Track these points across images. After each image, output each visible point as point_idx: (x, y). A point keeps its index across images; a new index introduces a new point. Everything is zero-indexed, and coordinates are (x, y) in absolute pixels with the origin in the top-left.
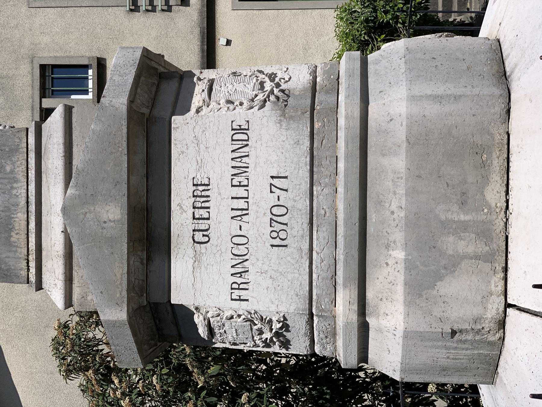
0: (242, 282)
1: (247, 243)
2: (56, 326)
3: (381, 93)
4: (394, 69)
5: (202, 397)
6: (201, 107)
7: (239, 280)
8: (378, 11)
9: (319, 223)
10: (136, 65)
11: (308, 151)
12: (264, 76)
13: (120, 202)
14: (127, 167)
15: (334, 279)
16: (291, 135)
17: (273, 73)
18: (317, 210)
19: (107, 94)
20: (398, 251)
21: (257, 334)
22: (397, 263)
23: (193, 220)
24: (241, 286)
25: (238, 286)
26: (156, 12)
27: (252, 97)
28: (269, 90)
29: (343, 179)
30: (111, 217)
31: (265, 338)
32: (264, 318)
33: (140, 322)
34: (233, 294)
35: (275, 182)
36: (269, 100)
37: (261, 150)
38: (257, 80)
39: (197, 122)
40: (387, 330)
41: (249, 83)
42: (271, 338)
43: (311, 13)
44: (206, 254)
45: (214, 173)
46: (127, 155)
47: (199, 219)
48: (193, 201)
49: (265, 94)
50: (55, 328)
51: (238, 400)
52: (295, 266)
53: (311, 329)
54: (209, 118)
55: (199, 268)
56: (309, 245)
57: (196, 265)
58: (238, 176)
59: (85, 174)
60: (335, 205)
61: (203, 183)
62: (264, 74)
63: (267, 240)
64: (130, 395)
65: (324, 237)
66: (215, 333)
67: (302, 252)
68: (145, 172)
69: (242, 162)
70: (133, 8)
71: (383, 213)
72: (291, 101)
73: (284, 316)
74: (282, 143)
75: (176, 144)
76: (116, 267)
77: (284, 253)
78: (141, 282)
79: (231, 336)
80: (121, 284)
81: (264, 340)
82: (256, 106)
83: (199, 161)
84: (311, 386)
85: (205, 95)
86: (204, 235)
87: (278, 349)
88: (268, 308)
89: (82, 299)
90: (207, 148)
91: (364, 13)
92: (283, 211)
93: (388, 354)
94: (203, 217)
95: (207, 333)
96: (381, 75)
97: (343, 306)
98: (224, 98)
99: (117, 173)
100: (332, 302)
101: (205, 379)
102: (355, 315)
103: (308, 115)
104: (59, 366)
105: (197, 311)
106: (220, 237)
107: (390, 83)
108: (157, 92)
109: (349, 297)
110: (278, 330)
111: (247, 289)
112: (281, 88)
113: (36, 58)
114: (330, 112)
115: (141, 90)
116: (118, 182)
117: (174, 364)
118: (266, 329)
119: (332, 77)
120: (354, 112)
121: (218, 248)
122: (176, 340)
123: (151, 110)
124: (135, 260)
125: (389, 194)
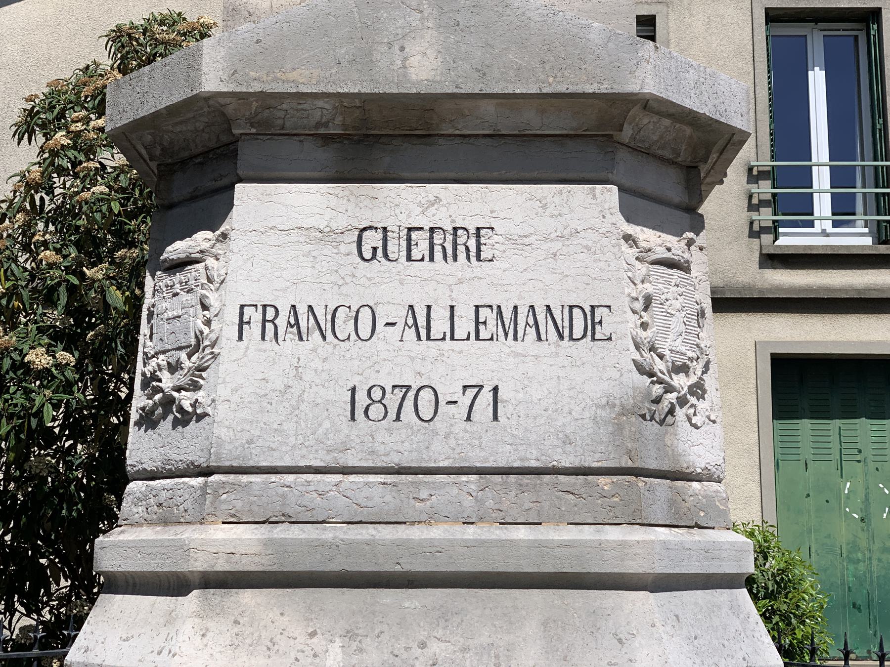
0: (278, 329)
1: (360, 338)
2: (205, 20)
3: (675, 618)
4: (723, 645)
5: (67, 277)
6: (636, 245)
7: (282, 322)
8: (768, 601)
9: (400, 486)
10: (717, 117)
11: (552, 464)
12: (699, 373)
13: (443, 79)
14: (515, 94)
15: (283, 519)
16: (584, 429)
17: (704, 391)
18: (428, 482)
19: (661, 55)
20: (340, 658)
21: (170, 360)
22: (315, 656)
23: (406, 228)
24: (269, 327)
25: (271, 318)
26: (748, 211)
27: (657, 348)
28: (672, 383)
29: (494, 537)
30: (414, 61)
31: (161, 377)
32: (203, 373)
33: (197, 124)
34: (253, 308)
35: (486, 396)
36: (653, 383)
37: (551, 365)
38: (691, 359)
39: (607, 235)
40: (170, 636)
41: (685, 342)
42: (161, 390)
43: (754, 481)
44: (337, 254)
45: (504, 271)
46: (539, 92)
47: (409, 239)
48: (445, 228)
49: (664, 374)
50: (202, 18)
51: (61, 344)
52: (310, 439)
53: (179, 473)
54: (615, 261)
55: (308, 240)
56: (355, 467)
57: (314, 234)
58: (497, 320)
59: (500, 9)
60: (438, 521)
61: (483, 248)
62: (703, 373)
63: (365, 378)
64: (75, 147)
65: (372, 498)
66: (175, 274)
67: (341, 452)
68: (503, 132)
69: (526, 327)
70: (755, 173)
71: (422, 624)
72: (652, 427)
73: (206, 415)
74: (566, 410)
75: (561, 193)
76: (311, 71)
77: (339, 415)
78: (280, 122)
79: (167, 306)
80: (276, 79)
81: (157, 376)
82: (642, 356)
83: (526, 241)
84: (85, 481)
85: (661, 253)
86: (375, 249)
87: (139, 406)
88: (224, 382)
89: (247, 13)
90: (555, 255)
91: (763, 575)
92: (426, 412)
93: (121, 638)
94: (412, 247)
95: (175, 257)
96: (711, 618)
97: (224, 540)
98: (654, 291)
99: (503, 73)
100: (234, 516)
101: (99, 280)
102: (205, 565)
103: (627, 463)
104: (133, 24)
105: (219, 236)
106: (372, 282)
107: (696, 638)
108: (661, 159)
109: (244, 552)
110: (177, 402)
111: (263, 338)
112: (677, 407)
113: (665, 8)
114: (633, 510)
115: (666, 127)
116: (484, 74)
117: (126, 224)
118: (180, 378)
119: (702, 514)
120: (634, 560)
121: (348, 279)
122: (162, 199)
123: (629, 147)
124: (324, 111)
125: (462, 636)
